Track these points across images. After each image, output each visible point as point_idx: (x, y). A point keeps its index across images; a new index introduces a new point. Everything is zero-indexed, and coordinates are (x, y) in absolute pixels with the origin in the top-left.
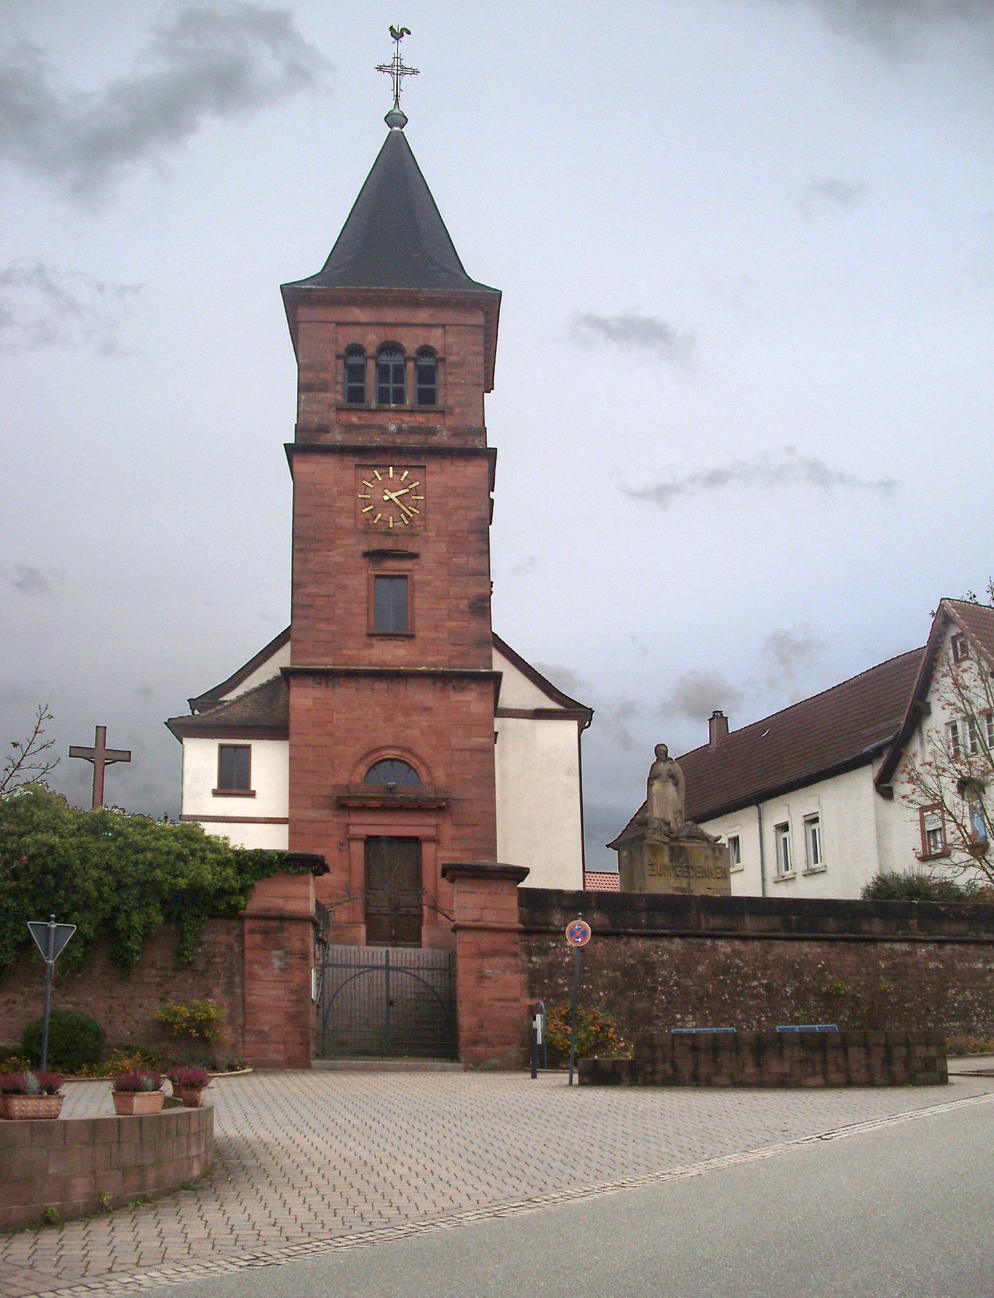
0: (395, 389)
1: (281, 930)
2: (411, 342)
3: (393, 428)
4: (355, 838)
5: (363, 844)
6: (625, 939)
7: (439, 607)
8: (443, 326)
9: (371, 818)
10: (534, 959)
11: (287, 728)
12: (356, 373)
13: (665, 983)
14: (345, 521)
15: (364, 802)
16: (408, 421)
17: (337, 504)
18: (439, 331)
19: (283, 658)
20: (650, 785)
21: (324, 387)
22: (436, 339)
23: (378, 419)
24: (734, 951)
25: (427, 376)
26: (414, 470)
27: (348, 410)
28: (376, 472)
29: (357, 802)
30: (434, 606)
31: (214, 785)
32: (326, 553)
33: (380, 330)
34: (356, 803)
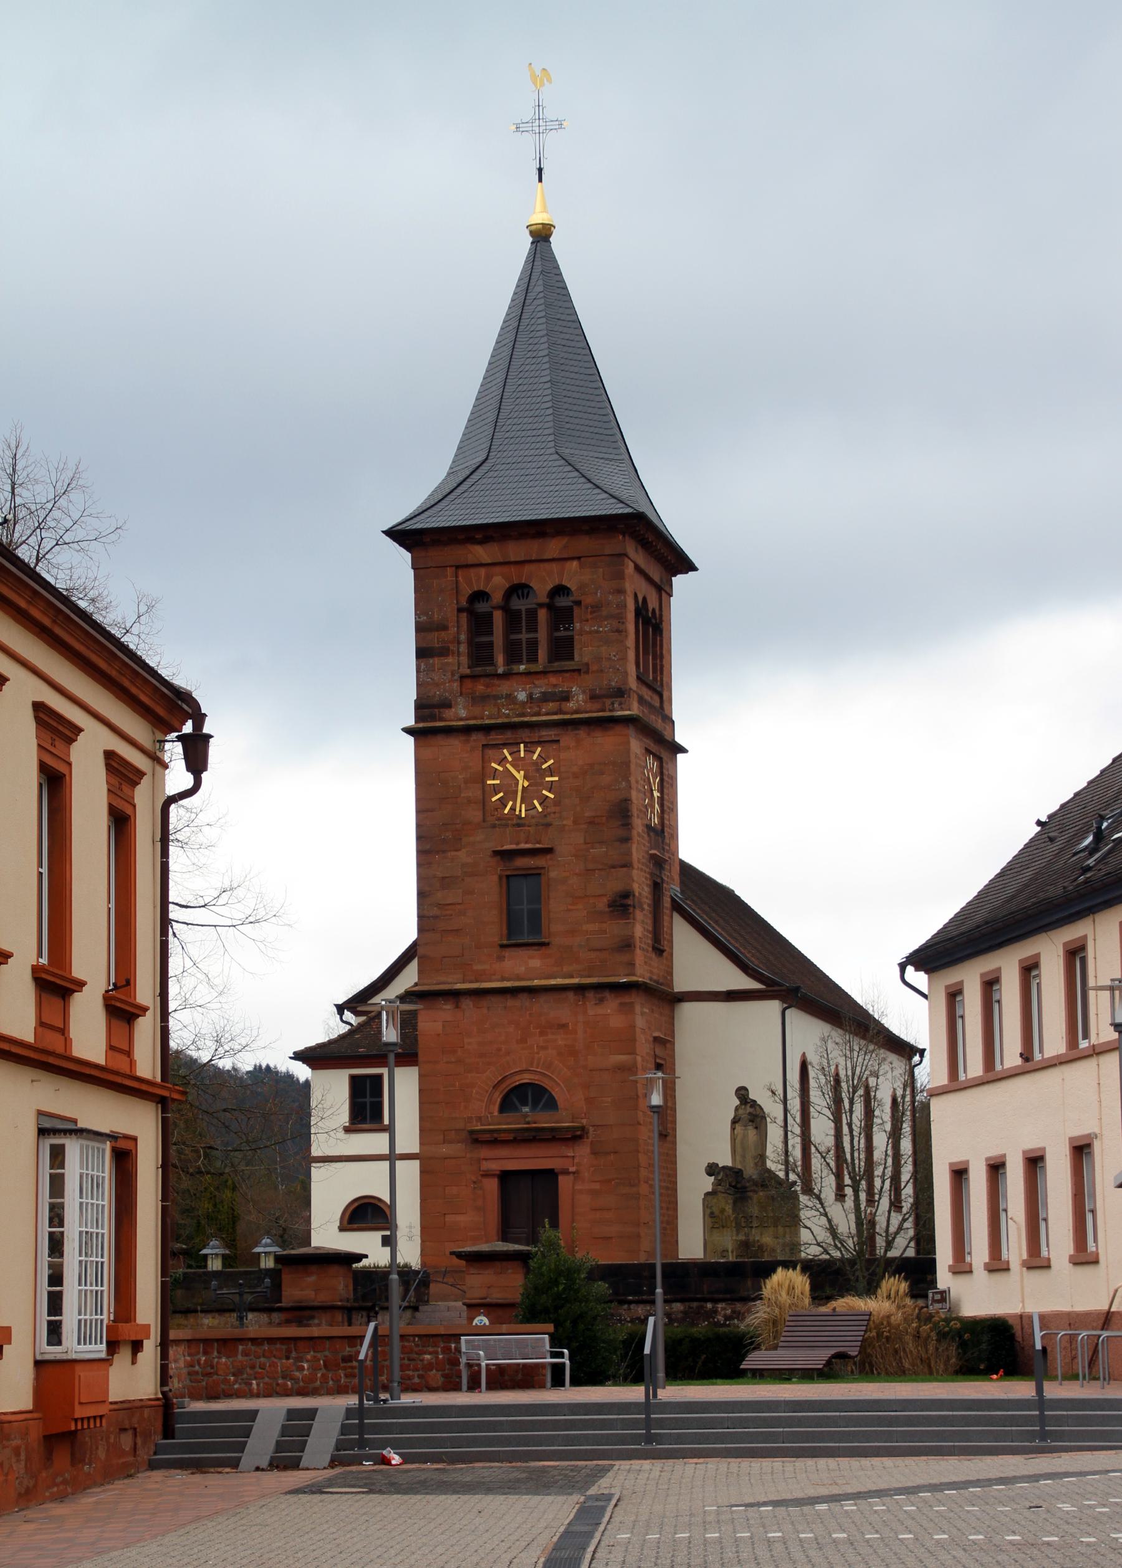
0: (528, 641)
2: (542, 583)
3: (522, 696)
4: (487, 1175)
5: (496, 1180)
6: (626, 1306)
8: (579, 558)
9: (504, 1152)
11: (416, 1055)
12: (480, 624)
14: (474, 814)
15: (496, 1135)
16: (541, 687)
17: (462, 795)
18: (575, 563)
19: (409, 979)
20: (733, 1129)
21: (444, 652)
22: (572, 575)
23: (504, 687)
24: (733, 1312)
25: (562, 616)
26: (547, 745)
27: (474, 677)
28: (505, 751)
29: (488, 1136)
30: (570, 907)
31: (344, 1118)
32: (453, 853)
33: (505, 569)
34: (487, 1137)
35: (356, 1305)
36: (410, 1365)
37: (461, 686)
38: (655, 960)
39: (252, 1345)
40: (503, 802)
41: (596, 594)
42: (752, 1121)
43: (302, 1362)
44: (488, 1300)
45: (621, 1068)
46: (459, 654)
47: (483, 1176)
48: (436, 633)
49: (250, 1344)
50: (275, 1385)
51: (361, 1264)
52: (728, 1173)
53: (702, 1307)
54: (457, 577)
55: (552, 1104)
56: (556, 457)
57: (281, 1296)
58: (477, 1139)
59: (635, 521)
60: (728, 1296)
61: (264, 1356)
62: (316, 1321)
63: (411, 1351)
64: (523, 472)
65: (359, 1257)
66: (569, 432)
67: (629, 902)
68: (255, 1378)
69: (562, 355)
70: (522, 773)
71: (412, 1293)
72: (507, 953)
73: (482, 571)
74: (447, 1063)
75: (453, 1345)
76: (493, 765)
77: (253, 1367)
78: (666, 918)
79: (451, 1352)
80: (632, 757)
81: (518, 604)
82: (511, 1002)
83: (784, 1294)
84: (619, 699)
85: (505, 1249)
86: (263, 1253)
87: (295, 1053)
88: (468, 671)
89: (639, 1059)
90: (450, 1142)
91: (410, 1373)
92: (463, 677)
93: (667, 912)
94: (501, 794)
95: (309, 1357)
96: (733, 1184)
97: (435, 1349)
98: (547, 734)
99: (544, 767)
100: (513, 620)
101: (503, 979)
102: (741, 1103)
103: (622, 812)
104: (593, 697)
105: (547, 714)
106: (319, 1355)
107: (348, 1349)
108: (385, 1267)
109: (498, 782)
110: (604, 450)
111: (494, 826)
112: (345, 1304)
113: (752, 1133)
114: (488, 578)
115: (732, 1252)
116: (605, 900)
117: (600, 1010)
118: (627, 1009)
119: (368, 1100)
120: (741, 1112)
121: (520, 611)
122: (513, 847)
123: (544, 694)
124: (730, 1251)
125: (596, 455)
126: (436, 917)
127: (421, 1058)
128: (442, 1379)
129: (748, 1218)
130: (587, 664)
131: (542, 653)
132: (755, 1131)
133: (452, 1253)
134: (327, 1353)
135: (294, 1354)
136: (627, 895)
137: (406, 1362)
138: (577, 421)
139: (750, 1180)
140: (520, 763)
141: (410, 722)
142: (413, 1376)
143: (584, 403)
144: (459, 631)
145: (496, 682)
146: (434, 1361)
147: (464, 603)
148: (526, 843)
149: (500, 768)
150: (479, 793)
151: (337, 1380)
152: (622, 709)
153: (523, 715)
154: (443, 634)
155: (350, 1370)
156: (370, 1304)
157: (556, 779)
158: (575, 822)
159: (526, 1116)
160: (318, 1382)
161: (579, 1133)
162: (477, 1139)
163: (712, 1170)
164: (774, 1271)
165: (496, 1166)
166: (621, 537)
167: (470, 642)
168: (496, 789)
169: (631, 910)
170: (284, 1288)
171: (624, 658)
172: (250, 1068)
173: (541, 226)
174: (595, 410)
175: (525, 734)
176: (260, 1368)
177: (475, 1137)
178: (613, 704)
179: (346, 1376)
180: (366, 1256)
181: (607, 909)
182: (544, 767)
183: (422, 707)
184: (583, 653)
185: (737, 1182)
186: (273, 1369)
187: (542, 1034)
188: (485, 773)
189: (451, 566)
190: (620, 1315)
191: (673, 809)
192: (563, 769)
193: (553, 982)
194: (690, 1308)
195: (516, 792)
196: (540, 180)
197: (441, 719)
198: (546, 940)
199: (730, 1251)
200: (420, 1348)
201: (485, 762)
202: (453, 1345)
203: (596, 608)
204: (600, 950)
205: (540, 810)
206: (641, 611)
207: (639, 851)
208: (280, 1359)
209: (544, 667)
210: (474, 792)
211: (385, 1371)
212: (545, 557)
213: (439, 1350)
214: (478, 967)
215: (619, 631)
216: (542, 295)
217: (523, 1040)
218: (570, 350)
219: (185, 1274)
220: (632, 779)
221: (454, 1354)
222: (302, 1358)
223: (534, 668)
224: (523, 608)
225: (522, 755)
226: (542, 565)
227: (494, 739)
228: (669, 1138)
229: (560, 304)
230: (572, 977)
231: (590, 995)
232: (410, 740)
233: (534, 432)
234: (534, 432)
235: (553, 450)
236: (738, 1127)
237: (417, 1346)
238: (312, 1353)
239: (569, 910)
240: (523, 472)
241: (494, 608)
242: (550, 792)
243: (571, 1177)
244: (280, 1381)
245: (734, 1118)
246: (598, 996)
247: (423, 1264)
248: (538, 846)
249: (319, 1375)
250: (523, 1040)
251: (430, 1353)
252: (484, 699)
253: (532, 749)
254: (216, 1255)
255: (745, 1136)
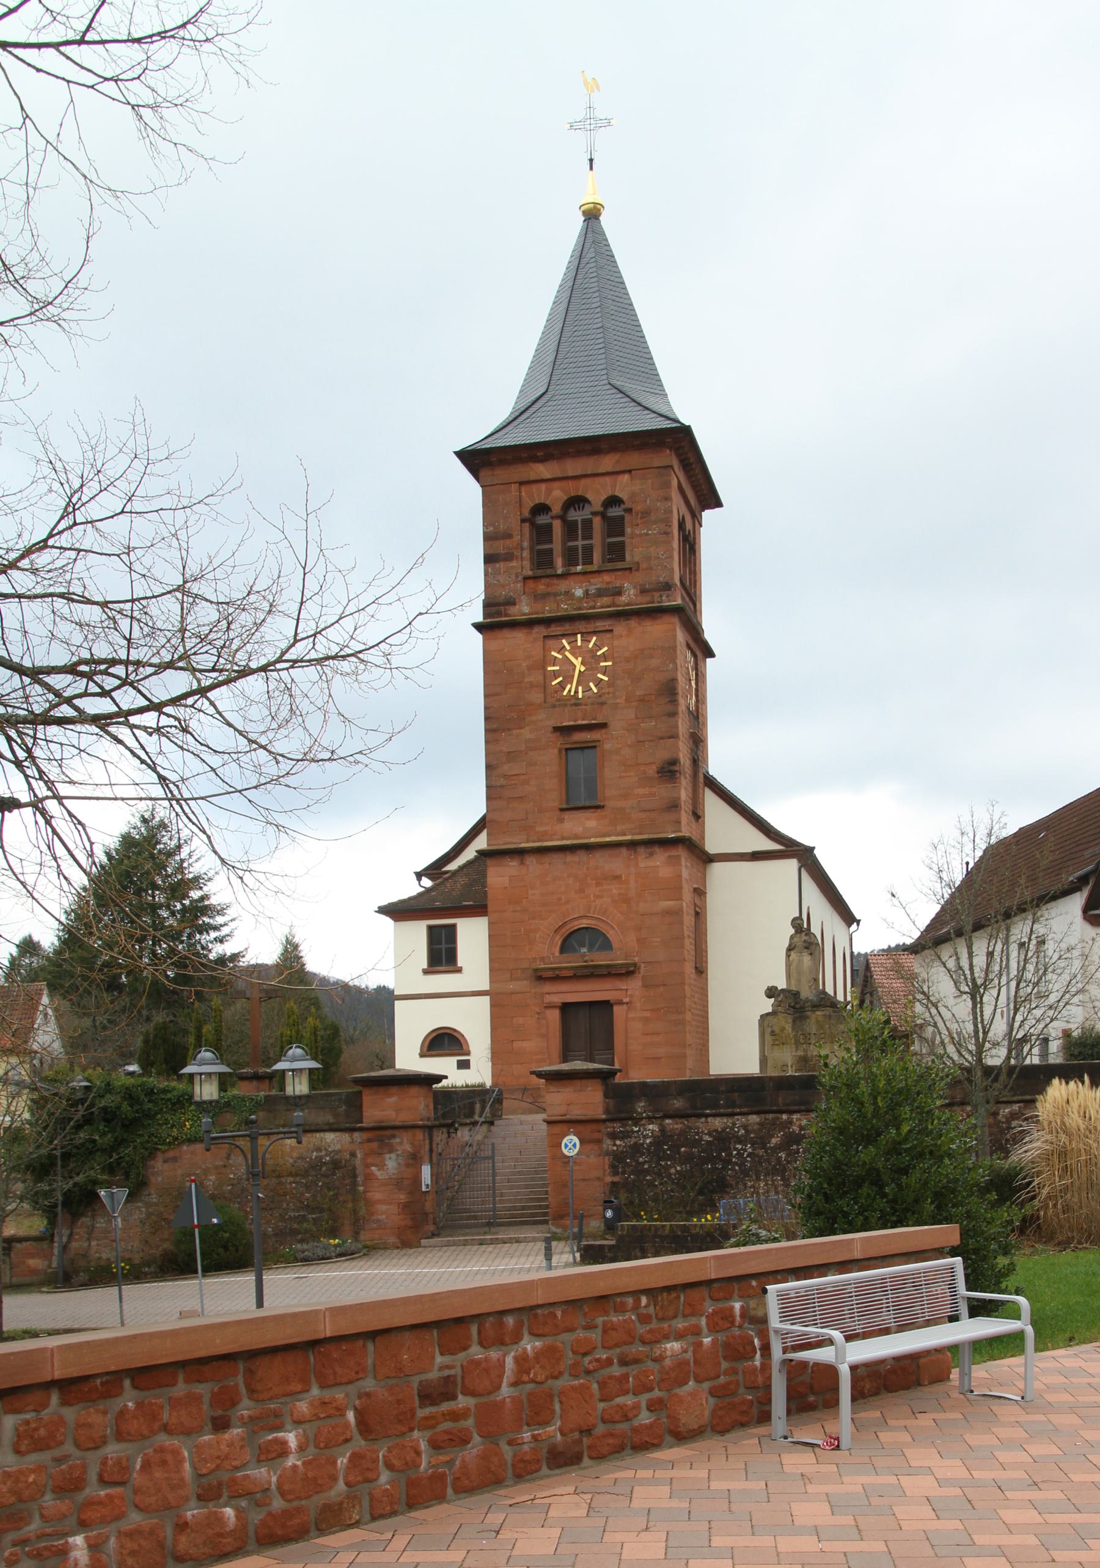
0: (584, 547)
1: (394, 1136)
2: (596, 493)
3: (579, 592)
4: (550, 1006)
6: (703, 1120)
7: (628, 774)
8: (630, 471)
10: (618, 1142)
12: (542, 533)
13: (740, 1155)
14: (536, 697)
15: (557, 972)
16: (597, 583)
17: (526, 680)
18: (626, 477)
19: (481, 842)
20: (788, 956)
21: (508, 557)
22: (623, 487)
23: (562, 586)
25: (615, 527)
26: (601, 634)
27: (535, 578)
30: (623, 774)
32: (517, 731)
33: (563, 484)
34: (550, 974)
35: (437, 1123)
36: (626, 1377)
37: (524, 585)
38: (694, 824)
39: (65, 1403)
40: (562, 684)
41: (646, 501)
42: (807, 948)
43: (280, 1428)
44: (568, 1117)
45: (668, 912)
46: (522, 559)
47: (546, 1007)
48: (502, 542)
49: (55, 1398)
50: (169, 1531)
51: (440, 1085)
52: (787, 994)
53: (778, 1119)
54: (520, 492)
55: (607, 945)
56: (609, 387)
57: (362, 1115)
58: (540, 977)
59: (682, 435)
60: (803, 1108)
61: (120, 1437)
62: (398, 1140)
63: (631, 1337)
64: (579, 400)
65: (439, 1078)
66: (619, 368)
67: (676, 768)
68: (83, 1525)
69: (612, 307)
70: (580, 659)
71: (488, 1109)
72: (567, 815)
73: (543, 486)
74: (514, 911)
75: (737, 1306)
76: (553, 653)
77: (70, 1485)
78: (701, 791)
79: (733, 1323)
80: (678, 644)
81: (574, 515)
82: (570, 858)
83: (1075, 1116)
84: (667, 592)
85: (585, 1067)
86: (289, 1070)
87: (379, 907)
88: (530, 573)
89: (684, 904)
90: (517, 979)
91: (628, 1400)
92: (526, 579)
93: (701, 786)
94: (561, 679)
95: (303, 1407)
96: (792, 1005)
97: (693, 1321)
98: (601, 625)
99: (599, 653)
100: (570, 530)
101: (563, 838)
102: (796, 932)
103: (670, 690)
104: (643, 591)
105: (602, 607)
106: (339, 1394)
107: (439, 1359)
108: (462, 1087)
109: (557, 668)
110: (650, 386)
111: (554, 706)
112: (426, 1123)
113: (807, 959)
114: (549, 491)
115: (792, 1066)
116: (654, 767)
117: (650, 863)
118: (674, 861)
119: (444, 946)
120: (796, 940)
121: (576, 521)
122: (572, 723)
123: (599, 590)
124: (789, 1065)
125: (643, 389)
126: (502, 787)
127: (490, 908)
128: (712, 1401)
129: (807, 1036)
130: (638, 563)
131: (597, 556)
132: (809, 957)
133: (533, 1073)
134: (369, 1384)
135: (245, 1408)
136: (674, 762)
137: (616, 1370)
138: (626, 360)
139: (807, 1000)
140: (577, 651)
141: (480, 618)
142: (636, 1407)
143: (632, 347)
144: (523, 537)
145: (555, 581)
146: (689, 1355)
147: (526, 514)
148: (583, 720)
149: (560, 656)
150: (541, 678)
151: (404, 1466)
152: (670, 601)
153: (580, 609)
154: (508, 542)
155: (447, 1425)
156: (450, 1121)
157: (610, 663)
158: (627, 700)
159: (584, 955)
160: (341, 1486)
161: (632, 969)
162: (540, 977)
163: (771, 992)
164: (1048, 1082)
165: (558, 999)
166: (668, 451)
167: (532, 549)
168: (555, 675)
169: (678, 775)
170: (364, 1110)
171: (671, 557)
172: (375, 987)
173: (592, 205)
174: (641, 354)
175: (582, 626)
176: (103, 1481)
177: (539, 974)
178: (661, 596)
179: (436, 1445)
180: (446, 1077)
181: (657, 775)
182: (599, 653)
183: (489, 605)
184: (632, 554)
185: (796, 1003)
186: (158, 1474)
187: (598, 884)
188: (546, 661)
189: (515, 483)
190: (698, 1128)
191: (704, 702)
192: (616, 655)
193: (608, 839)
194: (766, 1119)
195: (573, 676)
196: (591, 169)
197: (506, 615)
198: (602, 804)
199: (789, 1065)
200: (654, 1325)
201: (546, 651)
202: (737, 1306)
203: (646, 513)
204: (649, 811)
205: (595, 691)
206: (682, 525)
207: (683, 726)
208: (188, 1432)
209: (599, 567)
210: (536, 677)
211: (557, 1407)
212: (600, 471)
213: (703, 1321)
214: (539, 829)
215: (666, 533)
216: (593, 260)
217: (581, 891)
218: (619, 304)
219: (266, 1097)
220: (678, 662)
221: (740, 1327)
222: (277, 1414)
223: (589, 568)
224: (579, 519)
225: (579, 644)
226: (597, 480)
227: (555, 631)
228: (704, 975)
229: (609, 268)
230: (625, 834)
231: (641, 850)
232: (478, 637)
233: (589, 369)
234: (589, 369)
235: (606, 382)
236: (793, 955)
237: (645, 1319)
238: (315, 1391)
239: (621, 777)
240: (579, 400)
241: (552, 518)
242: (604, 675)
243: (625, 1006)
244: (192, 1513)
245: (790, 946)
246: (648, 850)
247: (494, 1084)
248: (593, 722)
249: (342, 1462)
250: (581, 891)
251: (679, 1336)
252: (545, 596)
253: (588, 638)
254: (209, 1074)
255: (800, 962)
